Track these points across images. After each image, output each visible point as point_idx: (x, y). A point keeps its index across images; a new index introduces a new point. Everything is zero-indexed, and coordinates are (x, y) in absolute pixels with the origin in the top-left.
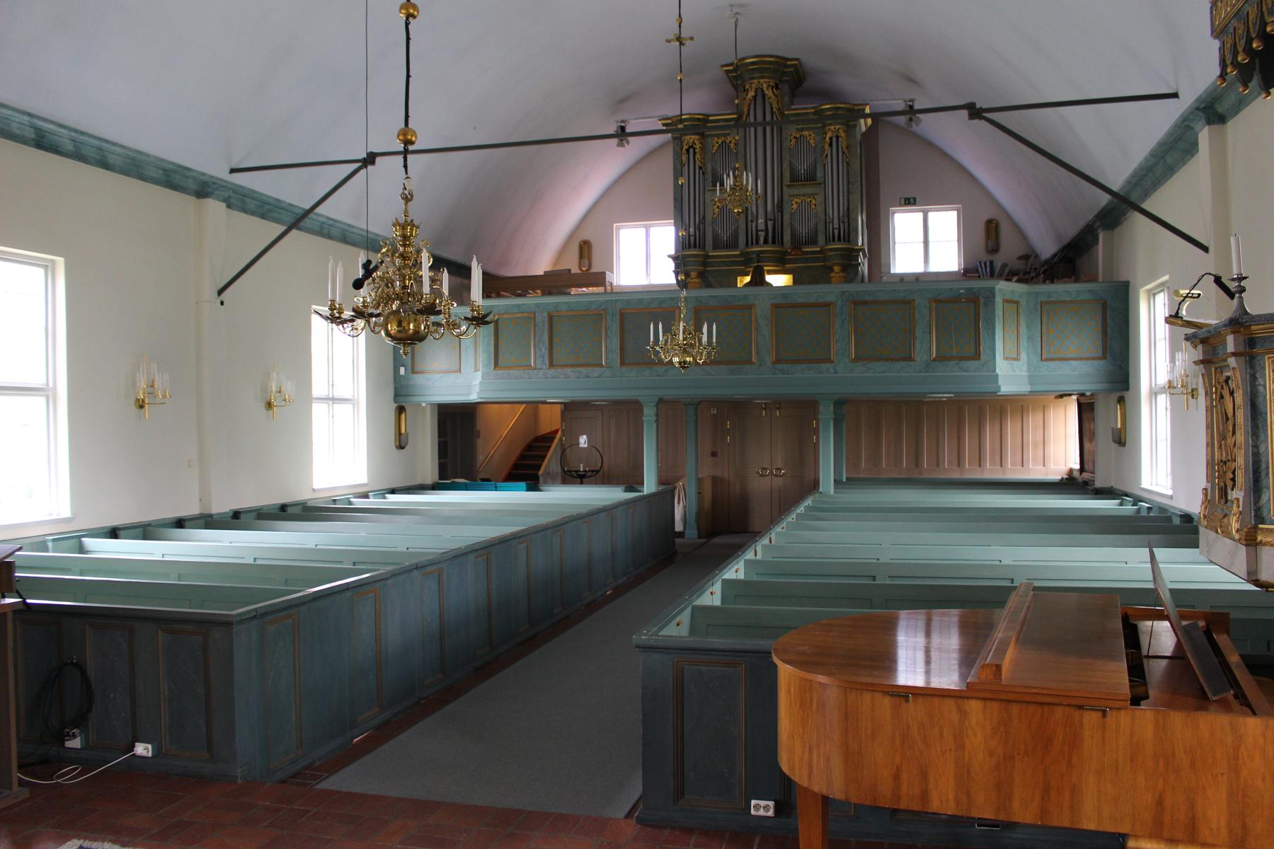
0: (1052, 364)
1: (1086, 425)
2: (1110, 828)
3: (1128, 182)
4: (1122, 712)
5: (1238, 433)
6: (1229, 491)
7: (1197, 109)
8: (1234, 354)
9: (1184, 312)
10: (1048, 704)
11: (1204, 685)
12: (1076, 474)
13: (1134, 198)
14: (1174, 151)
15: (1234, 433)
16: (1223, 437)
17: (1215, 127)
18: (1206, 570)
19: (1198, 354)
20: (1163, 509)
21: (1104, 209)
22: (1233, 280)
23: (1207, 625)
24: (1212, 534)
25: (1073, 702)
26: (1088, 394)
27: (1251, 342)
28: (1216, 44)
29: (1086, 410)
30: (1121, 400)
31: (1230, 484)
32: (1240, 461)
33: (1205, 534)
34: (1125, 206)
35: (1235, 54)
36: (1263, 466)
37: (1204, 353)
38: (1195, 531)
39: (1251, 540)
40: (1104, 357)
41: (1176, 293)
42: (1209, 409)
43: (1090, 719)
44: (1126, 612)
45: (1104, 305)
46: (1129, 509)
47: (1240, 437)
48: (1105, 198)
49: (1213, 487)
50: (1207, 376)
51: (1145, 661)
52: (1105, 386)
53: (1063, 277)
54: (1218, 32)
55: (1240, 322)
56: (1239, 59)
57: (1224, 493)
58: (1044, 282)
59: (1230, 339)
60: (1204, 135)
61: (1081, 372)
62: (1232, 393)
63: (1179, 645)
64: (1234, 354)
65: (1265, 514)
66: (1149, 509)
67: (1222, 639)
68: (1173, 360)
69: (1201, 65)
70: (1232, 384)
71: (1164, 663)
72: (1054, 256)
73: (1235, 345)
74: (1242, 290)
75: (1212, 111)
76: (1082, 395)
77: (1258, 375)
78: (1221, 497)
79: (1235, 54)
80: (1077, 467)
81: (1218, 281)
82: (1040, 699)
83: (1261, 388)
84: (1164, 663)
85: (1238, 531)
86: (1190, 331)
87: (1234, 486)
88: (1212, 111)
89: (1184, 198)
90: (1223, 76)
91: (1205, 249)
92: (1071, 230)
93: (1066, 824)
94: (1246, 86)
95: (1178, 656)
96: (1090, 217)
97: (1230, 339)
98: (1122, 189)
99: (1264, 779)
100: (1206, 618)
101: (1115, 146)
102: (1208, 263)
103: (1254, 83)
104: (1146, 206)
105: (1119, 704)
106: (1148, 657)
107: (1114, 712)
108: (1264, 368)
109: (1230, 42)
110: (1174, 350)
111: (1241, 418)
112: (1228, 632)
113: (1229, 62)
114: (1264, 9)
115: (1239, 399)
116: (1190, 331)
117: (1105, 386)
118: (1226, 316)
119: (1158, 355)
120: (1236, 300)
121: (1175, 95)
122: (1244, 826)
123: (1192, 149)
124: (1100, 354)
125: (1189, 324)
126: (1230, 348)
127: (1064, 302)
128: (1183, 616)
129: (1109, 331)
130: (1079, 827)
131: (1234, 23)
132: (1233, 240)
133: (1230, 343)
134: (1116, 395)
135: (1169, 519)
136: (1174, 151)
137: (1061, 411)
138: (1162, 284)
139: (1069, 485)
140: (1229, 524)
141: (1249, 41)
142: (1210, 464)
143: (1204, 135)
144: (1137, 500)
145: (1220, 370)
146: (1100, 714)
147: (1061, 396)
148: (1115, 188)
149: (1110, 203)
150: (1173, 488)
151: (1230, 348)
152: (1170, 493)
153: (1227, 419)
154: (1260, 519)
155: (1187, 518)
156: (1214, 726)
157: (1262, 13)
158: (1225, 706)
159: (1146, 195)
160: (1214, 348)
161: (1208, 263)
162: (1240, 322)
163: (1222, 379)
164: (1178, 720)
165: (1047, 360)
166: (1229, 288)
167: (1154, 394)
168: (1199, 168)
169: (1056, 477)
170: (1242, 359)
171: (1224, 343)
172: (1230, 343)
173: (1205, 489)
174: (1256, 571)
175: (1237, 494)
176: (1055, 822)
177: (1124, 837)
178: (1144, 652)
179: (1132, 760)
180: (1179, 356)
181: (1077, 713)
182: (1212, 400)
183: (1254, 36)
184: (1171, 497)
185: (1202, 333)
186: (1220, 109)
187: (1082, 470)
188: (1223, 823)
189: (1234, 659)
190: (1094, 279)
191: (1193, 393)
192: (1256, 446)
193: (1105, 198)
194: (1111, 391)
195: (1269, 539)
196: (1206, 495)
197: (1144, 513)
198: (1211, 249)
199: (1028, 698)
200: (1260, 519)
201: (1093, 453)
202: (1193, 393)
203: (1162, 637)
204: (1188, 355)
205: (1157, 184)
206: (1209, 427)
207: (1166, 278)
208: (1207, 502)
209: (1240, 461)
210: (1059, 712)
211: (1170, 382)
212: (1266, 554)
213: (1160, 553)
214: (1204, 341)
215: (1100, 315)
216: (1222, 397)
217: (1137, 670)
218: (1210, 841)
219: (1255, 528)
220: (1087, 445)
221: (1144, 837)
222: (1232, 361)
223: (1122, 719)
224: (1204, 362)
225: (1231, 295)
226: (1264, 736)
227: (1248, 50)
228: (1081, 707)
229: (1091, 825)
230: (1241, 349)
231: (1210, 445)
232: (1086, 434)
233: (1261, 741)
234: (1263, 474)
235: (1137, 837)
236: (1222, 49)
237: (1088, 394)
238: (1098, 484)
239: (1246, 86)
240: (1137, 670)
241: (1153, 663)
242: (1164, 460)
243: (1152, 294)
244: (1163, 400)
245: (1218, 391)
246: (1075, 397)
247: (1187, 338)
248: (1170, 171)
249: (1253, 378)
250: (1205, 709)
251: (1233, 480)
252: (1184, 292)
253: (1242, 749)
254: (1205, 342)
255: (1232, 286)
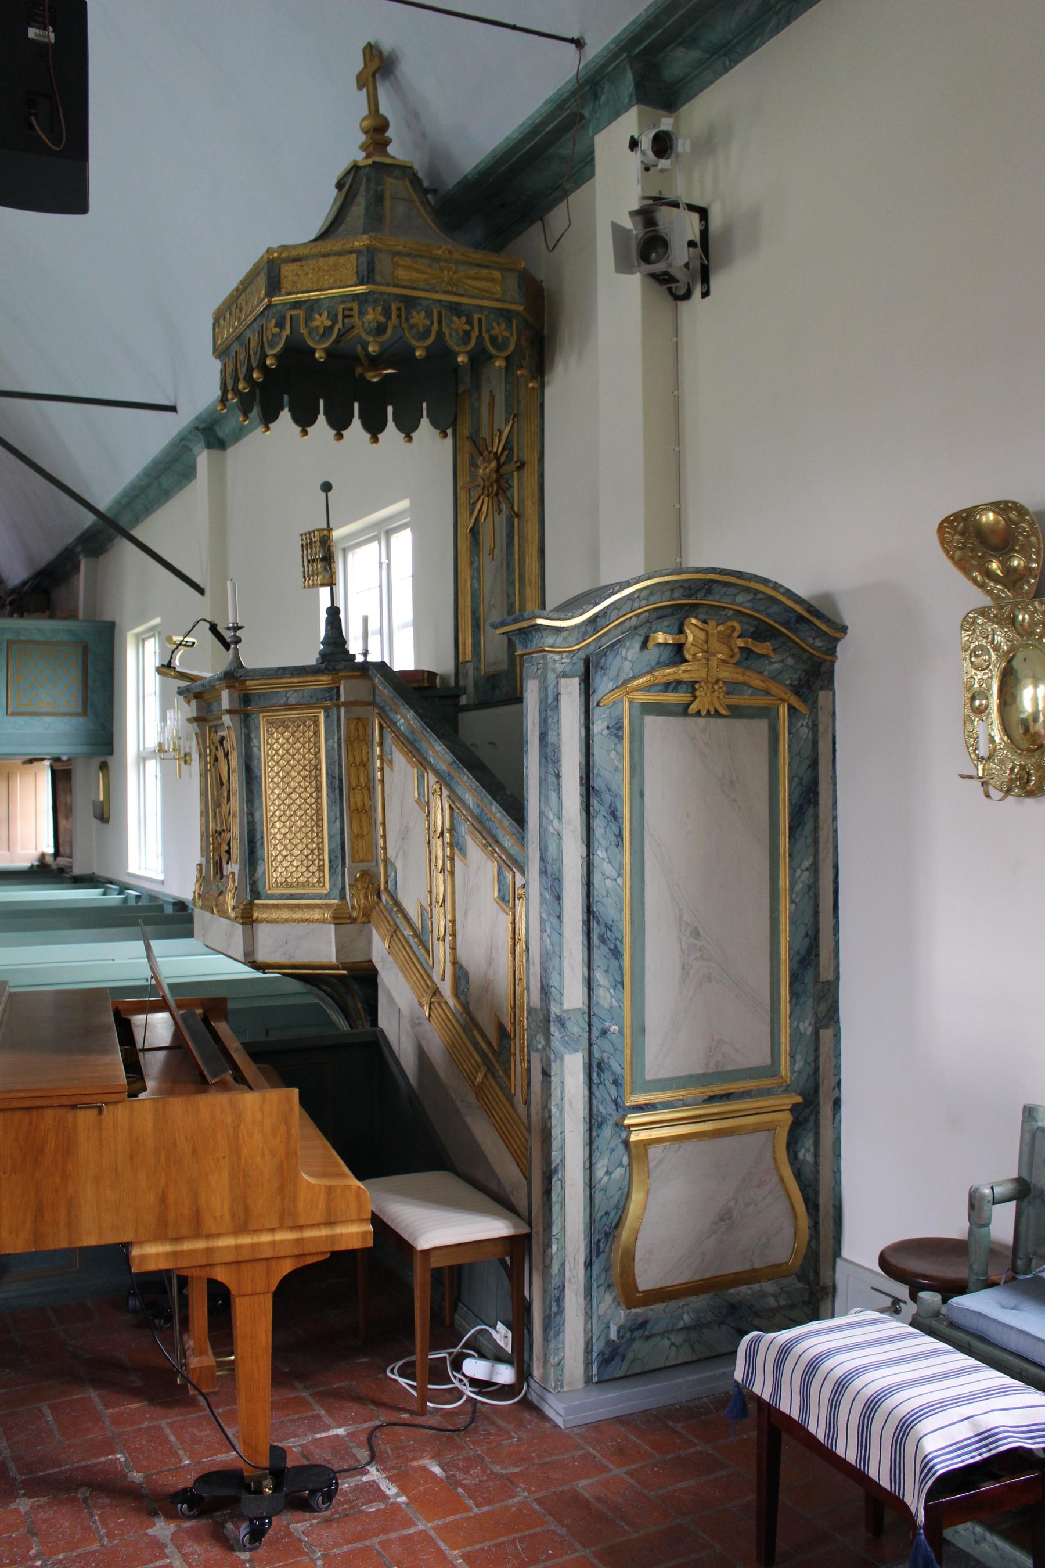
0: (20, 720)
1: (61, 797)
2: (111, 1238)
3: (117, 502)
4: (120, 1105)
5: (233, 799)
6: (224, 865)
7: (197, 428)
8: (229, 712)
9: (177, 662)
10: (38, 1108)
11: (203, 1067)
12: (49, 860)
13: (123, 521)
14: (169, 474)
15: (229, 800)
16: (218, 805)
17: (215, 452)
18: (203, 960)
19: (191, 710)
20: (153, 897)
21: (87, 531)
22: (229, 629)
23: (204, 1013)
24: (208, 914)
25: (65, 1102)
26: (65, 758)
27: (246, 699)
28: (218, 365)
29: (61, 779)
30: (104, 766)
31: (225, 856)
32: (235, 830)
33: (201, 917)
34: (112, 531)
35: (236, 380)
36: (258, 836)
37: (198, 709)
38: (190, 920)
39: (247, 918)
40: (84, 713)
41: (169, 639)
42: (203, 774)
43: (85, 1118)
44: (118, 1011)
45: (85, 648)
46: (114, 898)
47: (235, 804)
48: (90, 519)
49: (208, 862)
50: (201, 736)
51: (141, 1055)
52: (85, 749)
53: (30, 612)
54: (221, 352)
55: (235, 676)
56: (240, 387)
57: (219, 867)
58: (11, 615)
59: (225, 694)
60: (203, 459)
61: (55, 730)
62: (226, 755)
63: (177, 1034)
64: (229, 712)
65: (260, 888)
66: (138, 897)
67: (222, 1028)
68: (164, 719)
69: (202, 386)
70: (227, 745)
71: (162, 1054)
72: (25, 583)
73: (230, 702)
74: (238, 641)
75: (212, 434)
76: (56, 760)
77: (253, 735)
78: (216, 873)
79: (236, 380)
80: (51, 850)
81: (213, 628)
82: (28, 1103)
83: (255, 750)
84: (162, 1054)
85: (234, 908)
86: (183, 684)
87: (229, 859)
88: (212, 434)
89: (177, 527)
90: (223, 400)
91: (201, 591)
92: (46, 554)
93: (64, 1245)
94: (246, 417)
95: (177, 1045)
96: (70, 539)
97: (225, 694)
98: (110, 509)
99: (263, 1155)
100: (203, 1009)
101: (107, 458)
102: (202, 607)
103: (255, 412)
104: (135, 533)
105: (117, 1097)
106: (144, 1050)
107: (111, 1107)
108: (258, 728)
109: (231, 367)
110: (165, 706)
111: (235, 779)
112: (226, 1020)
113: (230, 387)
114: (265, 340)
115: (234, 762)
116: (183, 684)
117: (85, 749)
118: (221, 668)
119: (148, 714)
120: (231, 651)
121: (173, 409)
122: (246, 1209)
123: (189, 474)
124: (80, 710)
125: (183, 676)
126: (225, 704)
127: (37, 643)
128: (180, 1005)
129: (90, 682)
130: (80, 1244)
131: (236, 347)
132: (229, 584)
133: (225, 699)
134: (96, 762)
135: (161, 908)
136: (169, 474)
137: (30, 779)
138: (152, 629)
139: (42, 872)
140: (225, 902)
141: (250, 370)
142: (205, 835)
143: (203, 459)
144: (123, 888)
145: (215, 729)
146: (95, 1112)
147: (31, 761)
148: (102, 507)
149: (94, 525)
150: (165, 871)
151: (225, 704)
152: (161, 877)
153: (222, 784)
154: (256, 894)
155: (181, 906)
156: (214, 1106)
157: (263, 343)
158: (223, 1087)
159: (137, 520)
160: (209, 704)
161: (202, 607)
162: (235, 676)
163: (218, 738)
164: (177, 1106)
165: (13, 714)
166: (226, 639)
167: (142, 759)
168: (193, 501)
169: (25, 864)
170: (237, 717)
171: (219, 699)
172: (225, 699)
173: (200, 865)
174: (253, 952)
175: (232, 868)
176: (51, 1245)
177: (127, 1245)
178: (139, 1046)
179: (132, 1158)
180: (171, 714)
181: (70, 1114)
182: (206, 766)
183: (254, 365)
184: (163, 882)
185: (196, 687)
186: (222, 432)
187: (57, 854)
188: (226, 1207)
189: (234, 1045)
190: (72, 615)
191: (186, 758)
192: (251, 814)
193: (90, 519)
194: (90, 755)
195: (264, 916)
196: (200, 871)
197: (132, 902)
198: (207, 592)
199: (15, 1104)
200: (256, 894)
201: (70, 833)
202: (186, 758)
203: (158, 1028)
204: (181, 712)
205: (149, 509)
206: (204, 793)
207: (157, 621)
208: (202, 879)
209: (235, 830)
210: (49, 1114)
211: (160, 745)
212: (263, 932)
213: (155, 944)
214: (198, 696)
215: (80, 657)
216: (216, 759)
217: (134, 1068)
218: (214, 1231)
219: (251, 904)
220: (62, 823)
221: (148, 1241)
222: (227, 719)
223: (119, 1114)
224: (199, 719)
225: (227, 646)
226: (262, 1110)
227: (249, 379)
228: (74, 1107)
229: (90, 1240)
230: (236, 706)
231: (204, 814)
232: (61, 808)
233: (259, 1116)
234: (258, 844)
235: (141, 1243)
236: (223, 371)
237: (65, 758)
238: (77, 871)
239: (246, 417)
240: (134, 1068)
241: (149, 1055)
242: (153, 843)
243: (141, 639)
244: (153, 767)
245: (213, 753)
246: (47, 763)
247: (181, 692)
248: (166, 495)
249: (248, 739)
250: (205, 1091)
251: (228, 852)
252: (177, 639)
253: (242, 1127)
254: (198, 694)
255: (228, 635)
